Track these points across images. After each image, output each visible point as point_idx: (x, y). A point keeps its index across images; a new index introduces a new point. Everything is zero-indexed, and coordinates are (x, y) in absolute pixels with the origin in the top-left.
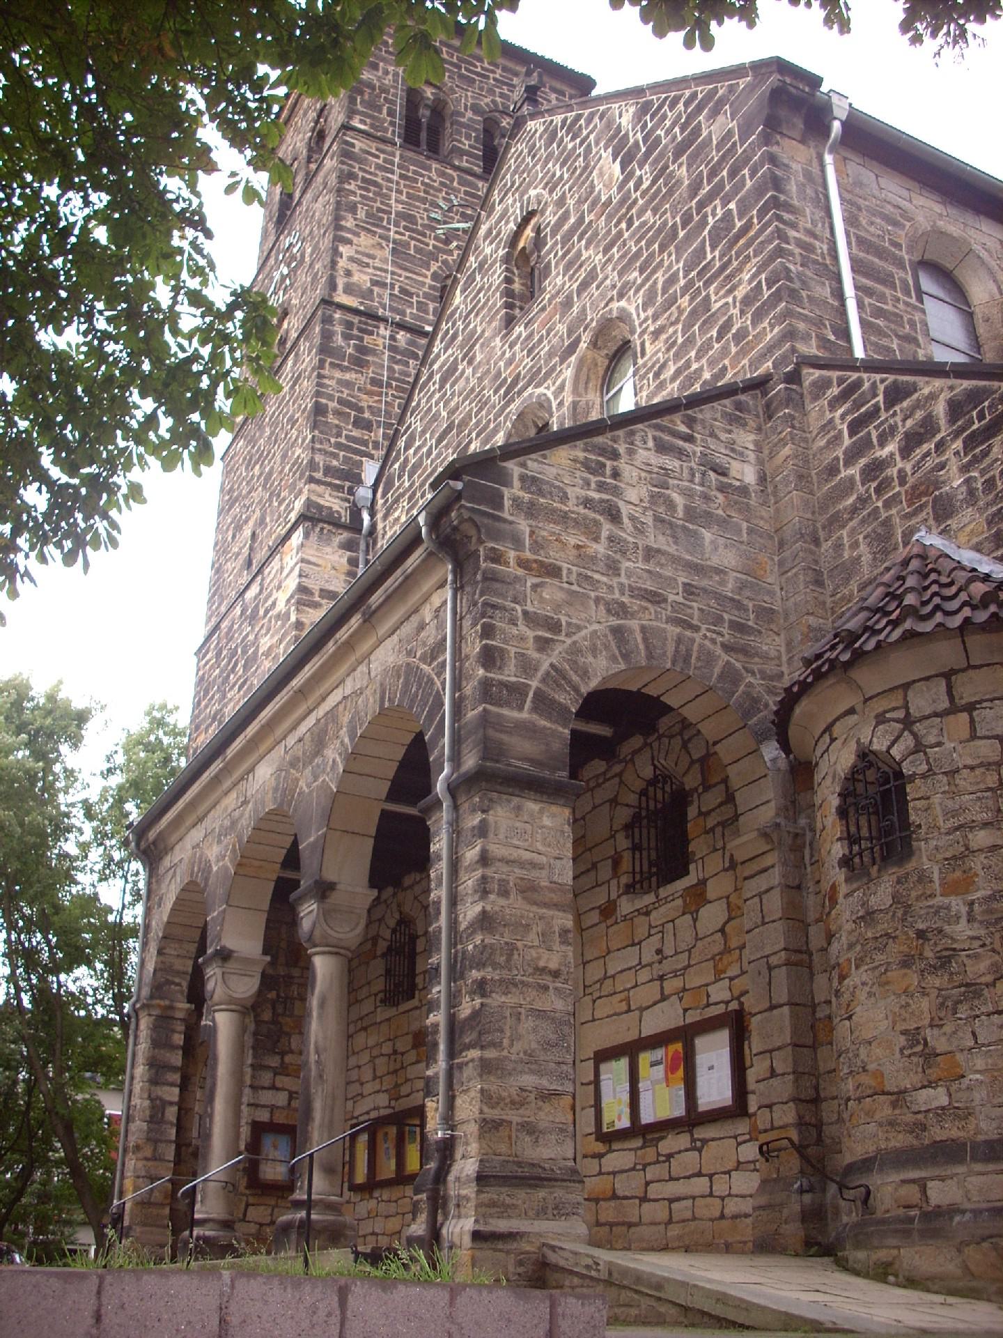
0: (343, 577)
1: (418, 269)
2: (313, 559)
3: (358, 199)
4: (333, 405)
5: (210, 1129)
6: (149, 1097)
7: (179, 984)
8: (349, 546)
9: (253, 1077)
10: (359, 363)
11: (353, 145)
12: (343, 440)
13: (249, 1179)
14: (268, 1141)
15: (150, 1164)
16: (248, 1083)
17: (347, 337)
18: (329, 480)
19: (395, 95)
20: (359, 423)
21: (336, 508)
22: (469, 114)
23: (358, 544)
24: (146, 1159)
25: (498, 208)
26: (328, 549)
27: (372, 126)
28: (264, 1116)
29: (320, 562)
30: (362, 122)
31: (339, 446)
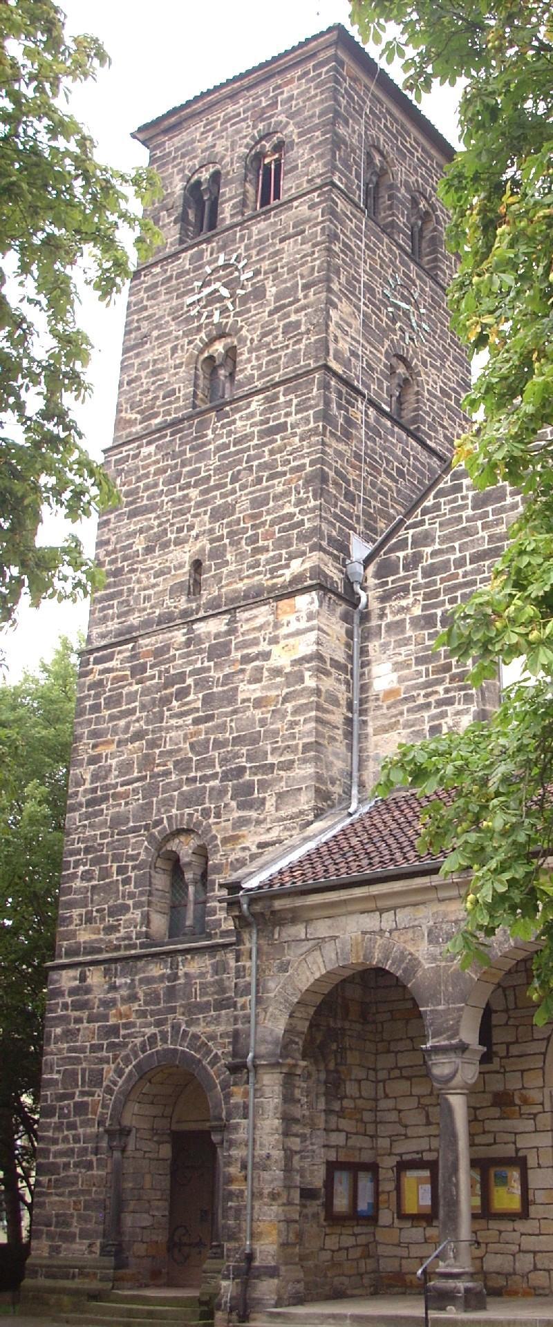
0: (343, 647)
1: (377, 345)
2: (325, 628)
3: (340, 262)
4: (332, 474)
5: (458, 1195)
6: (284, 1149)
7: (297, 1043)
8: (346, 618)
9: (326, 1121)
10: (347, 436)
11: (336, 204)
12: (338, 511)
13: (326, 1212)
14: (337, 1175)
15: (286, 1208)
16: (322, 1126)
17: (340, 407)
18: (331, 549)
19: (360, 157)
20: (350, 497)
21: (336, 579)
22: (403, 190)
23: (352, 617)
24: (284, 1205)
25: (272, 220)
26: (334, 620)
27: (346, 186)
28: (332, 1156)
29: (329, 631)
30: (340, 180)
31: (336, 516)
